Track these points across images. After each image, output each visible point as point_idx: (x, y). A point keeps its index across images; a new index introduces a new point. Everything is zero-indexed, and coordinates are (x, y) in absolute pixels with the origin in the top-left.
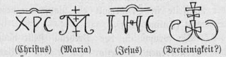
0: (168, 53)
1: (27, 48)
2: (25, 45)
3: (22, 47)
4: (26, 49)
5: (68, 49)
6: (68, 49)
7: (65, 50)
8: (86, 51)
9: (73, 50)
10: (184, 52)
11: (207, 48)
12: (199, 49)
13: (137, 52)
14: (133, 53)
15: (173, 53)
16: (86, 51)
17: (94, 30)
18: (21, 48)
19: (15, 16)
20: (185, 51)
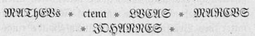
0: (27, 17)
1: (37, 12)
2: (34, 8)
3: (150, 11)
4: (36, 13)
5: (199, 13)
6: (199, 13)
7: (6, 15)
8: (104, 15)
9: (102, 15)
10: (92, 16)
11: (94, 12)
12: (104, 14)
13: (58, 16)
14: (98, 11)
15: (101, 11)
16: (104, 15)
17: (106, 11)
18: (228, 12)
19: (38, 8)
20: (93, 15)
